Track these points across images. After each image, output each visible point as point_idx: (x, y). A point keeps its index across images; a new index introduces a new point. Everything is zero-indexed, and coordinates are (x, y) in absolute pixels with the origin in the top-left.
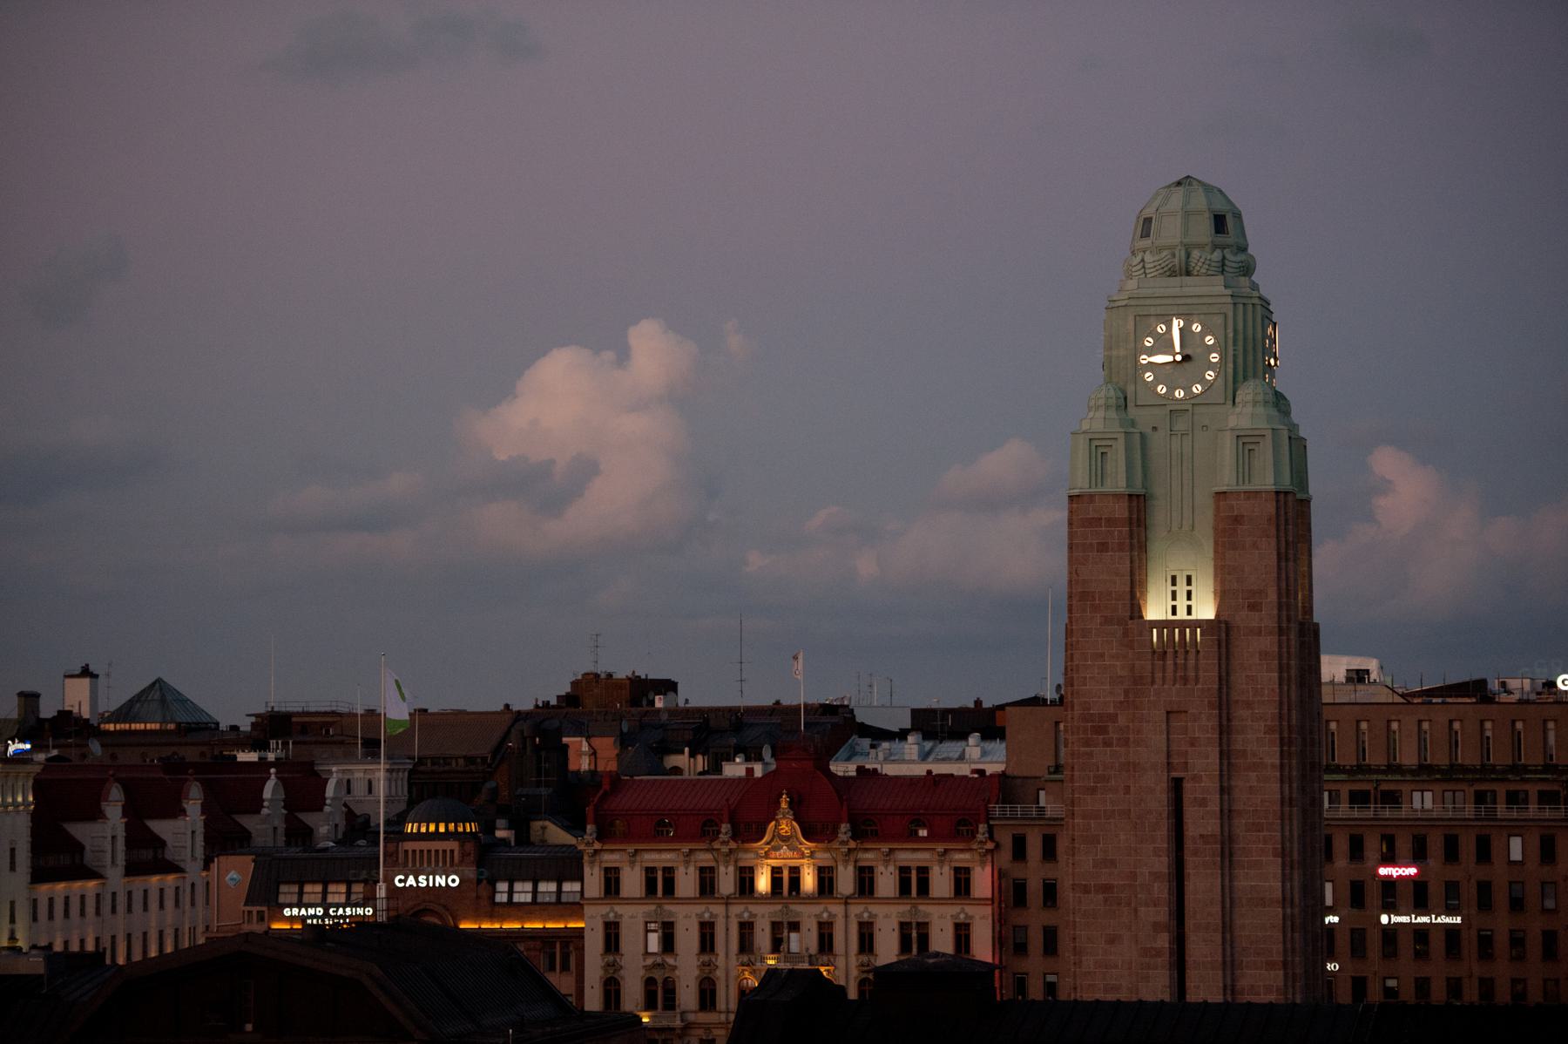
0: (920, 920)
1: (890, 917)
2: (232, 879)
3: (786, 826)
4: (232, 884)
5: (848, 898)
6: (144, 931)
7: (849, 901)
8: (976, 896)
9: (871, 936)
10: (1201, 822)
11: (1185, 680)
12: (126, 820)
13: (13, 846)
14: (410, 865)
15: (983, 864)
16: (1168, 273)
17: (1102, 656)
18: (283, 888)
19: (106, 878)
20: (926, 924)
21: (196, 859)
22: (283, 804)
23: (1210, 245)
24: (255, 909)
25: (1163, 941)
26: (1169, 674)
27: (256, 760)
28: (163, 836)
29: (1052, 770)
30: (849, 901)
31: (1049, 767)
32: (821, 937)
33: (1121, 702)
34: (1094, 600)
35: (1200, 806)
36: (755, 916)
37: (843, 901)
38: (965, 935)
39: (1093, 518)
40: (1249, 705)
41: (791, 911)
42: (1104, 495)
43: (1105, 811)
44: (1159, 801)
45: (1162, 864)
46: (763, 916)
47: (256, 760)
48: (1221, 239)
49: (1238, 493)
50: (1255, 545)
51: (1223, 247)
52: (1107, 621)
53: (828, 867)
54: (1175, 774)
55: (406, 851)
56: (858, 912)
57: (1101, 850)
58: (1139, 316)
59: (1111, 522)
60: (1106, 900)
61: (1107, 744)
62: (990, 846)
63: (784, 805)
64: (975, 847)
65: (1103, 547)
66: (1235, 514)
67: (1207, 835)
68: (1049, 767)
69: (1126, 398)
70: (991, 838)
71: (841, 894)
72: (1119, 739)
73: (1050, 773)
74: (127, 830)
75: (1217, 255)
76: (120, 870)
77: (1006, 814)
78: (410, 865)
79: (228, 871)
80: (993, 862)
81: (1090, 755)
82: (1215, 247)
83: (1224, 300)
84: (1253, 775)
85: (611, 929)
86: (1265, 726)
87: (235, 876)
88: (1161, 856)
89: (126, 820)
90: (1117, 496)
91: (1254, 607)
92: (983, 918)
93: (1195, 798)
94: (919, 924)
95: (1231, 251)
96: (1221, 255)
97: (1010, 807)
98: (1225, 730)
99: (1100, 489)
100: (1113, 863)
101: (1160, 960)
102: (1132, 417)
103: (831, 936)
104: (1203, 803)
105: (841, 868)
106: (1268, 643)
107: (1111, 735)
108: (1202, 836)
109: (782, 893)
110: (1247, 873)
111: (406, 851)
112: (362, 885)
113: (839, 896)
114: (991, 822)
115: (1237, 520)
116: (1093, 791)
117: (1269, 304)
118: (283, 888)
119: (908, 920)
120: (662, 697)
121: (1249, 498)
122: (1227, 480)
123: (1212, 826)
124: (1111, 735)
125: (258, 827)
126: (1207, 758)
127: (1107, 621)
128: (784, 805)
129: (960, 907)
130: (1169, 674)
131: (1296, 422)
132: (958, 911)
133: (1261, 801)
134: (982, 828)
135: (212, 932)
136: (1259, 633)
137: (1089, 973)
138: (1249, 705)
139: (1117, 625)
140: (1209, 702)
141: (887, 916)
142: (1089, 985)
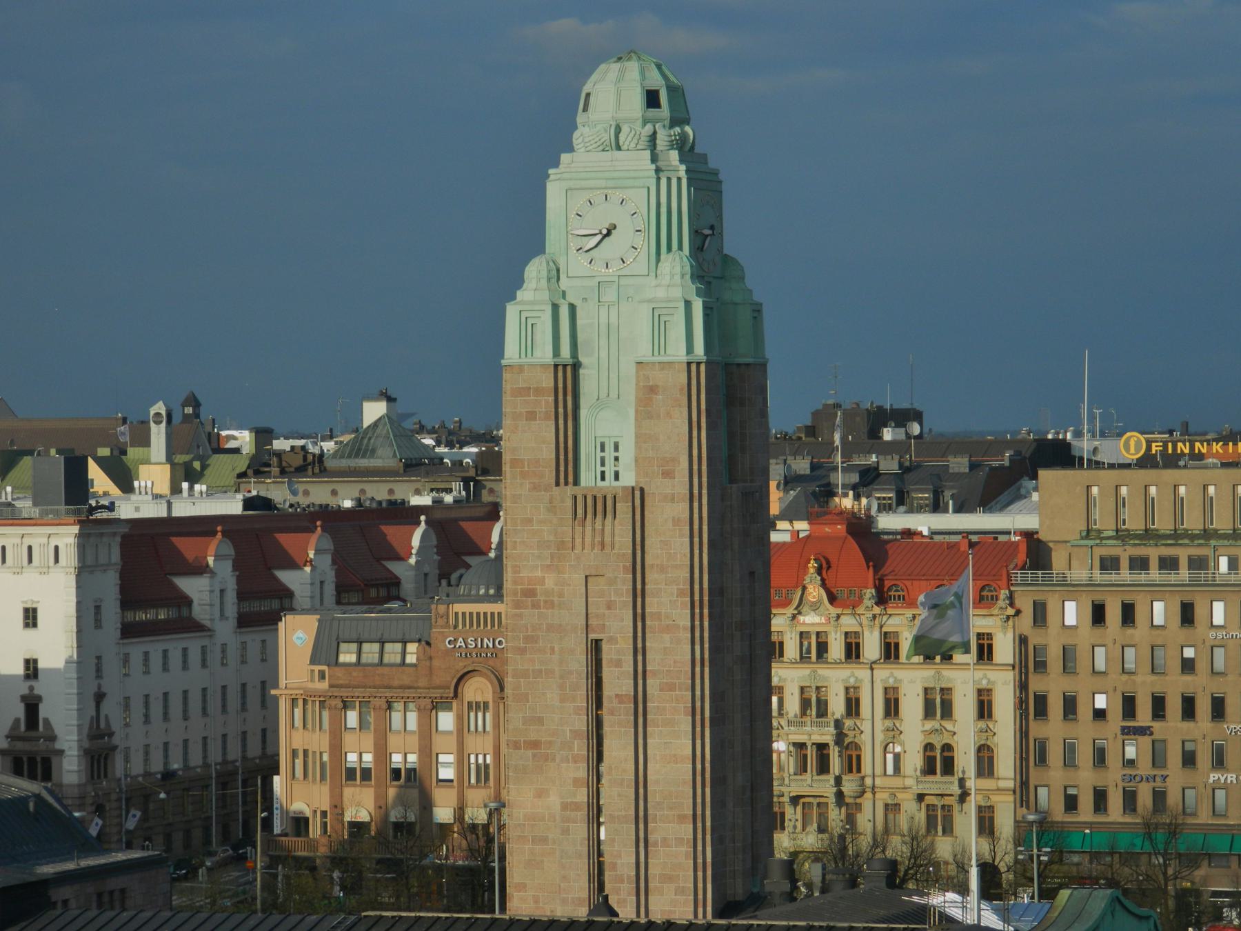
0: (943, 686)
1: (915, 682)
2: (299, 638)
3: (815, 591)
4: (298, 642)
5: (874, 662)
6: (146, 693)
7: (874, 666)
8: (999, 662)
9: (897, 701)
10: (617, 682)
11: (603, 545)
12: (237, 573)
13: (98, 604)
14: (460, 627)
15: (1005, 629)
16: (601, 148)
17: (530, 521)
18: (343, 646)
19: (214, 631)
20: (950, 689)
21: (227, 619)
22: (435, 550)
23: (641, 119)
24: (317, 668)
25: (582, 796)
26: (588, 539)
27: (430, 503)
28: (292, 587)
29: (1084, 534)
30: (874, 666)
31: (1081, 531)
32: (849, 701)
33: (548, 566)
34: (524, 467)
35: (616, 667)
36: (785, 680)
37: (869, 666)
38: (988, 701)
39: (523, 388)
40: (662, 569)
41: (820, 675)
42: (532, 366)
43: (533, 670)
44: (579, 662)
45: (580, 722)
46: (793, 681)
47: (430, 503)
48: (653, 112)
49: (654, 363)
50: (669, 415)
51: (654, 121)
52: (535, 488)
53: (855, 632)
54: (593, 636)
55: (456, 614)
56: (884, 678)
57: (530, 708)
58: (571, 189)
59: (539, 391)
60: (534, 756)
61: (535, 606)
62: (1011, 611)
63: (812, 571)
64: (996, 612)
65: (531, 416)
66: (651, 384)
67: (622, 695)
68: (1081, 531)
69: (558, 270)
70: (1012, 605)
71: (867, 659)
72: (546, 602)
73: (1082, 538)
74: (238, 583)
75: (649, 128)
76: (232, 622)
77: (1038, 581)
78: (460, 627)
79: (294, 630)
80: (1014, 627)
81: (520, 616)
82: (645, 122)
83: (647, 174)
84: (667, 637)
85: (984, 639)
86: (678, 589)
87: (301, 635)
88: (580, 715)
89: (237, 573)
90: (543, 366)
91: (668, 474)
92: (1005, 683)
93: (611, 659)
94: (942, 689)
95: (664, 126)
96: (652, 128)
97: (1032, 574)
98: (639, 594)
99: (530, 360)
100: (540, 720)
101: (579, 813)
102: (564, 289)
103: (858, 701)
104: (618, 664)
105: (867, 634)
106: (682, 509)
107: (539, 598)
108: (617, 696)
109: (810, 658)
110: (661, 731)
111: (456, 614)
112: (417, 644)
113: (865, 661)
114: (1012, 588)
115: (653, 390)
116: (522, 651)
117: (717, 174)
118: (343, 646)
119: (932, 686)
120: (890, 429)
121: (662, 369)
122: (644, 350)
123: (627, 686)
124: (539, 598)
125: (407, 573)
126: (622, 620)
127: (535, 488)
128: (812, 571)
129: (983, 672)
130: (588, 539)
131: (750, 288)
132: (981, 677)
133: (675, 662)
134: (1004, 593)
135: (281, 689)
136: (673, 500)
137: (519, 825)
138: (662, 569)
139: (545, 491)
140: (624, 567)
141: (912, 682)
142: (519, 836)
